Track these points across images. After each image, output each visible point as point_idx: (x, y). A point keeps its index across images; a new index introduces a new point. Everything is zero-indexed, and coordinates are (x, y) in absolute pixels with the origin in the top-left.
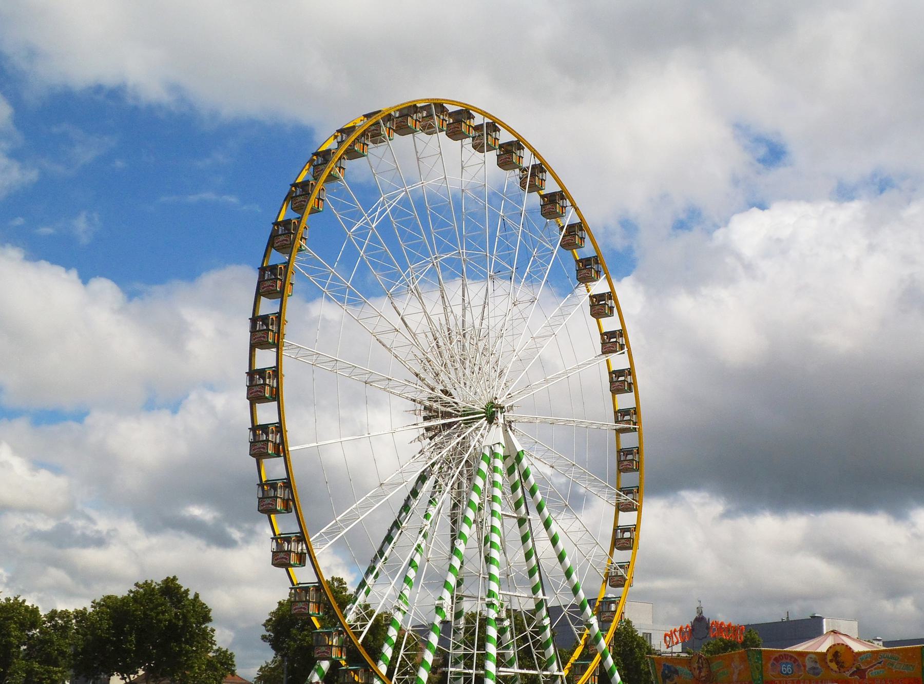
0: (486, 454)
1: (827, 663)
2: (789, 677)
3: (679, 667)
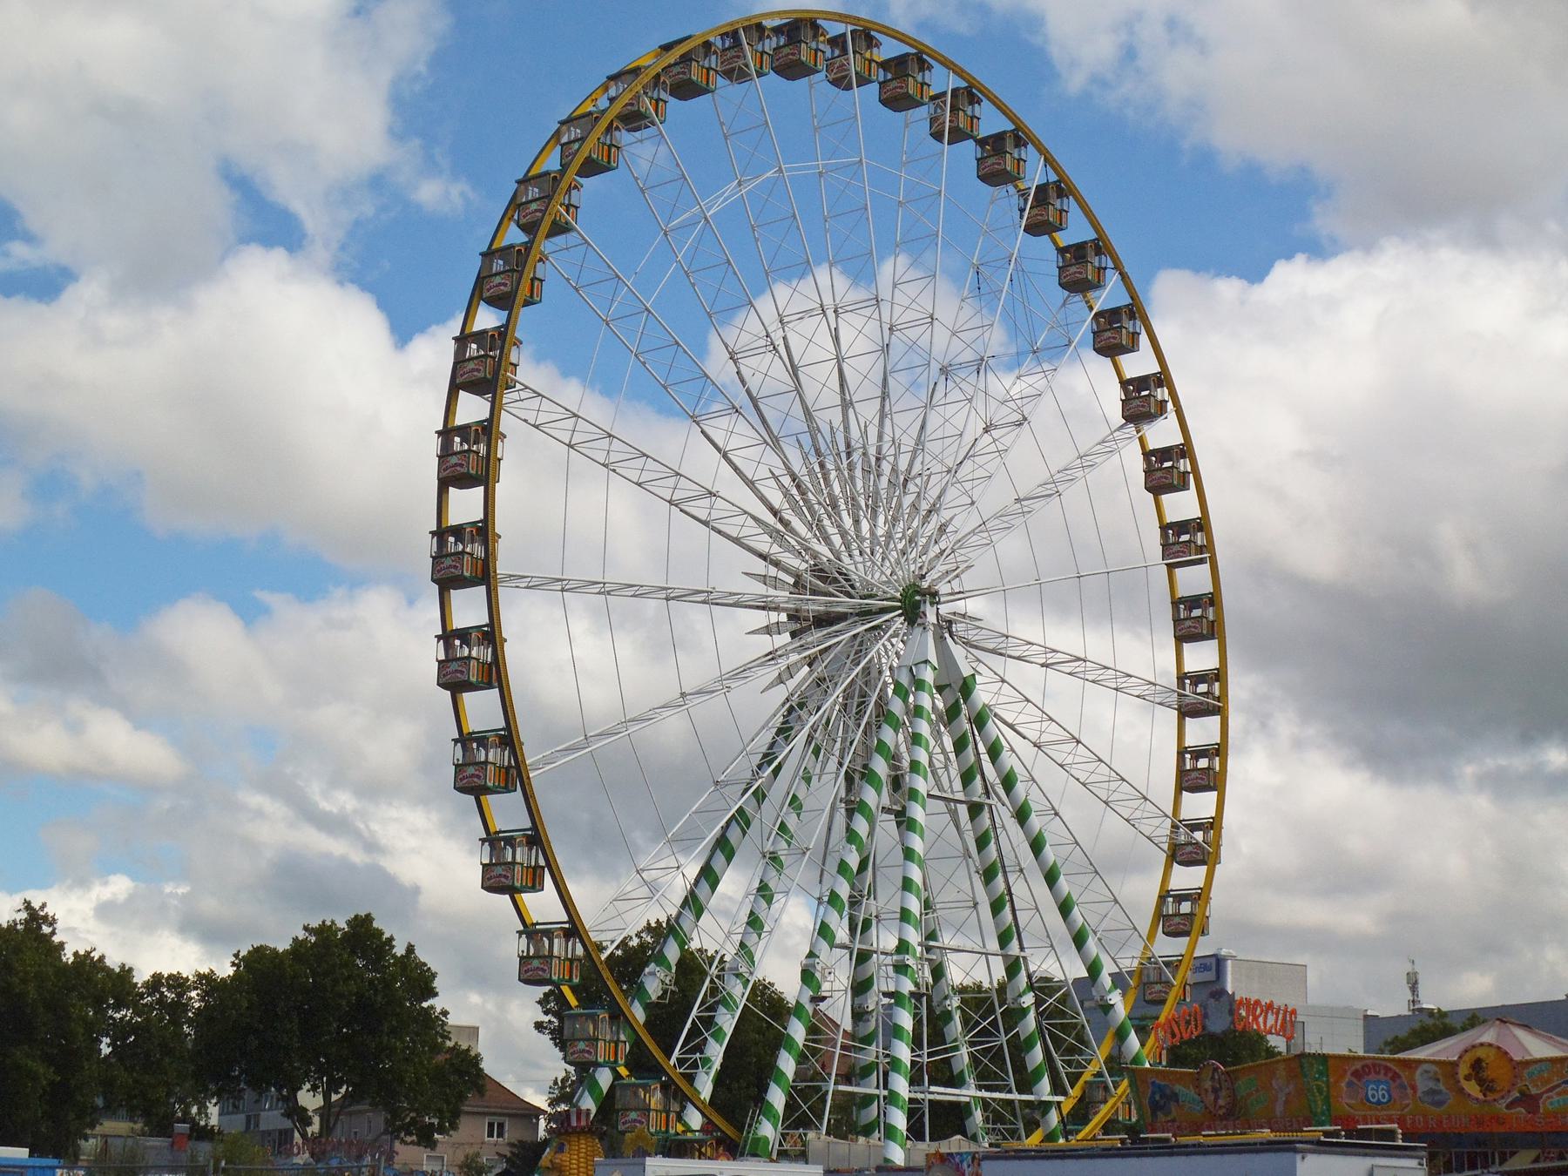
0: (901, 681)
1: (1459, 1082)
2: (1382, 1109)
3: (1178, 1088)
